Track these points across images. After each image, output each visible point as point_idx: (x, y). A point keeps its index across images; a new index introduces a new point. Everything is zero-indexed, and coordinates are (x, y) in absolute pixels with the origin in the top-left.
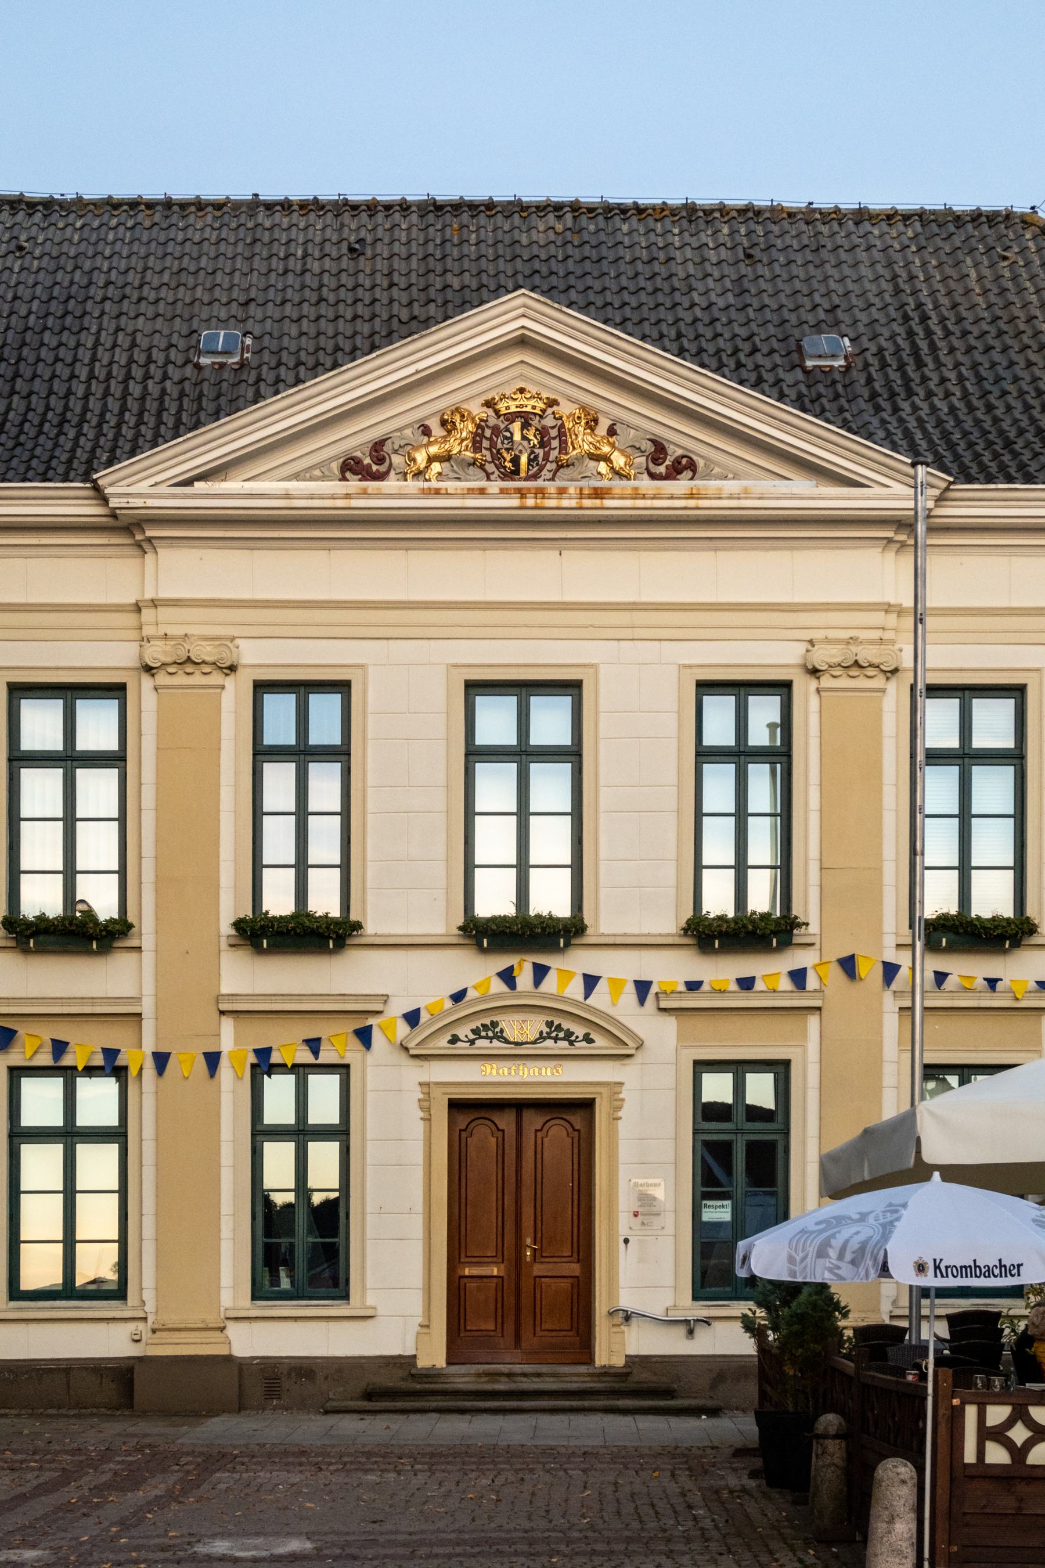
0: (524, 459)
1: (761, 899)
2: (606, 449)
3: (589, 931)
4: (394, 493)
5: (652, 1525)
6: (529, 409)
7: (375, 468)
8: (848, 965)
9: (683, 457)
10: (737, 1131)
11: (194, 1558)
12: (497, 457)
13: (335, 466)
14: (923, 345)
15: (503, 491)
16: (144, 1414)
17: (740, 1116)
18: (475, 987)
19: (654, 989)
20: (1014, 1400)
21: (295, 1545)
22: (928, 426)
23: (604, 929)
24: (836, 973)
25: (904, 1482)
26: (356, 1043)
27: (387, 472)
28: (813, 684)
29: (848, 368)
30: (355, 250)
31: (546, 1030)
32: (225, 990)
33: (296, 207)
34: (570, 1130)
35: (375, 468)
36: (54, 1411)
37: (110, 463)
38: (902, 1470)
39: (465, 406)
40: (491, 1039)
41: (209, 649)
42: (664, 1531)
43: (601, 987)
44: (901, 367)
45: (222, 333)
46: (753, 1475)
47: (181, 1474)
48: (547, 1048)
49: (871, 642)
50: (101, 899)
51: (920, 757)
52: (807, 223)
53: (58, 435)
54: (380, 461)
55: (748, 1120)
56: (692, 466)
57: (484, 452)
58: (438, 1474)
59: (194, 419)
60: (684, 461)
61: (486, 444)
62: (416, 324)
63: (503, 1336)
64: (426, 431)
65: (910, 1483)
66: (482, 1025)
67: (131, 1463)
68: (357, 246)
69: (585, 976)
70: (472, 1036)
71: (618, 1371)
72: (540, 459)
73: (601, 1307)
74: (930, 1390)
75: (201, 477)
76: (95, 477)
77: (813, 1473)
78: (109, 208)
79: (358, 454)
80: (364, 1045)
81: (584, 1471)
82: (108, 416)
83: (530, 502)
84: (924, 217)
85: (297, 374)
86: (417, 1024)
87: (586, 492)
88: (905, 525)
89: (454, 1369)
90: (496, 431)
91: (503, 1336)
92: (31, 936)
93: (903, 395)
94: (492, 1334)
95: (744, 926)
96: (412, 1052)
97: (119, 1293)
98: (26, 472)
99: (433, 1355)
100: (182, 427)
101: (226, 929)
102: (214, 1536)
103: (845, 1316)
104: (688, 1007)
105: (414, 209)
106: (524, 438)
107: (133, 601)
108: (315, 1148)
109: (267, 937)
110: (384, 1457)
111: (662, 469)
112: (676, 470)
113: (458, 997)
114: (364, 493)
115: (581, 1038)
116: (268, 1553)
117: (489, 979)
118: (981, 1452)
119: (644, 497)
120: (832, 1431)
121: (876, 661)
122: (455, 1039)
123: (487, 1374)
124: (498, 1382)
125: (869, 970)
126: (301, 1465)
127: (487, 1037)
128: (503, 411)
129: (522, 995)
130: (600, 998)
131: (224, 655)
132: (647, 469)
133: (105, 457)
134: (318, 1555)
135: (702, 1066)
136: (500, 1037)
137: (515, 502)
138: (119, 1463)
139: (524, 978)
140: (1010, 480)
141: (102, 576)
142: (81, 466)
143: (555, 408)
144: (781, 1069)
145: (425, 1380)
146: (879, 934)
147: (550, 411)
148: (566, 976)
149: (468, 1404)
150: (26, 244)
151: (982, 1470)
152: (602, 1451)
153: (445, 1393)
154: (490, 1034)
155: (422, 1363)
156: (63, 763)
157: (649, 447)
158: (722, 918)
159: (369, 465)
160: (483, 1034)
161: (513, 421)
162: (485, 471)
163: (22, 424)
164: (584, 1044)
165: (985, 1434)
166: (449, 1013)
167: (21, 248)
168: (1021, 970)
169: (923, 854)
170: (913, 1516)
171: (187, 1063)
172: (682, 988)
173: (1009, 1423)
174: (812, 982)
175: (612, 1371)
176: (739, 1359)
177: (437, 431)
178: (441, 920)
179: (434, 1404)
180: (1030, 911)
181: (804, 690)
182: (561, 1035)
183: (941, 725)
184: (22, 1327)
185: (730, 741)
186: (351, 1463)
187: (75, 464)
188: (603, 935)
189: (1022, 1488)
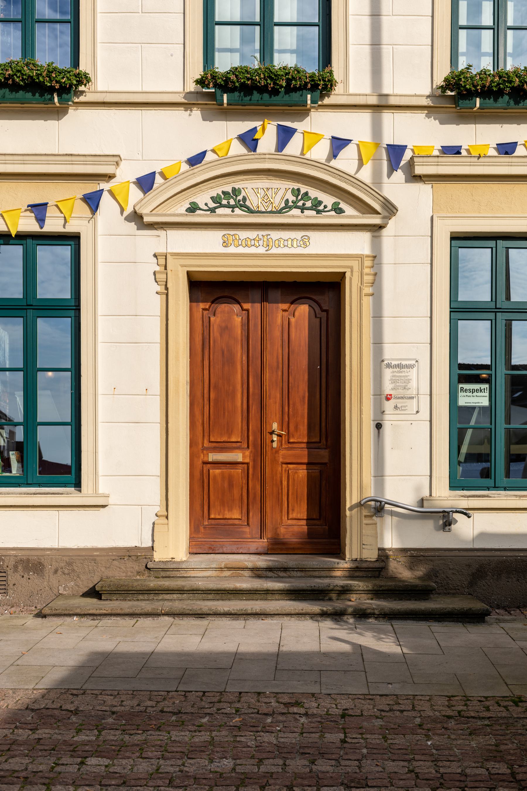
3: (338, 89)
18: (213, 151)
19: (407, 155)
26: (84, 209)
31: (291, 198)
40: (233, 207)
48: (293, 216)
63: (248, 524)
66: (223, 193)
70: (212, 205)
71: (371, 565)
73: (352, 497)
86: (151, 188)
91: (248, 524)
94: (237, 522)
96: (146, 219)
99: (174, 546)
108: (43, 326)
113: (196, 160)
115: (329, 207)
117: (229, 142)
122: (193, 208)
127: (228, 206)
129: (263, 157)
136: (243, 205)
139: (268, 140)
145: (163, 574)
153: (181, 591)
154: (232, 202)
155: (158, 556)
160: (224, 202)
166: (185, 175)
175: (365, 565)
176: (498, 553)
178: (174, 72)
182: (309, 204)
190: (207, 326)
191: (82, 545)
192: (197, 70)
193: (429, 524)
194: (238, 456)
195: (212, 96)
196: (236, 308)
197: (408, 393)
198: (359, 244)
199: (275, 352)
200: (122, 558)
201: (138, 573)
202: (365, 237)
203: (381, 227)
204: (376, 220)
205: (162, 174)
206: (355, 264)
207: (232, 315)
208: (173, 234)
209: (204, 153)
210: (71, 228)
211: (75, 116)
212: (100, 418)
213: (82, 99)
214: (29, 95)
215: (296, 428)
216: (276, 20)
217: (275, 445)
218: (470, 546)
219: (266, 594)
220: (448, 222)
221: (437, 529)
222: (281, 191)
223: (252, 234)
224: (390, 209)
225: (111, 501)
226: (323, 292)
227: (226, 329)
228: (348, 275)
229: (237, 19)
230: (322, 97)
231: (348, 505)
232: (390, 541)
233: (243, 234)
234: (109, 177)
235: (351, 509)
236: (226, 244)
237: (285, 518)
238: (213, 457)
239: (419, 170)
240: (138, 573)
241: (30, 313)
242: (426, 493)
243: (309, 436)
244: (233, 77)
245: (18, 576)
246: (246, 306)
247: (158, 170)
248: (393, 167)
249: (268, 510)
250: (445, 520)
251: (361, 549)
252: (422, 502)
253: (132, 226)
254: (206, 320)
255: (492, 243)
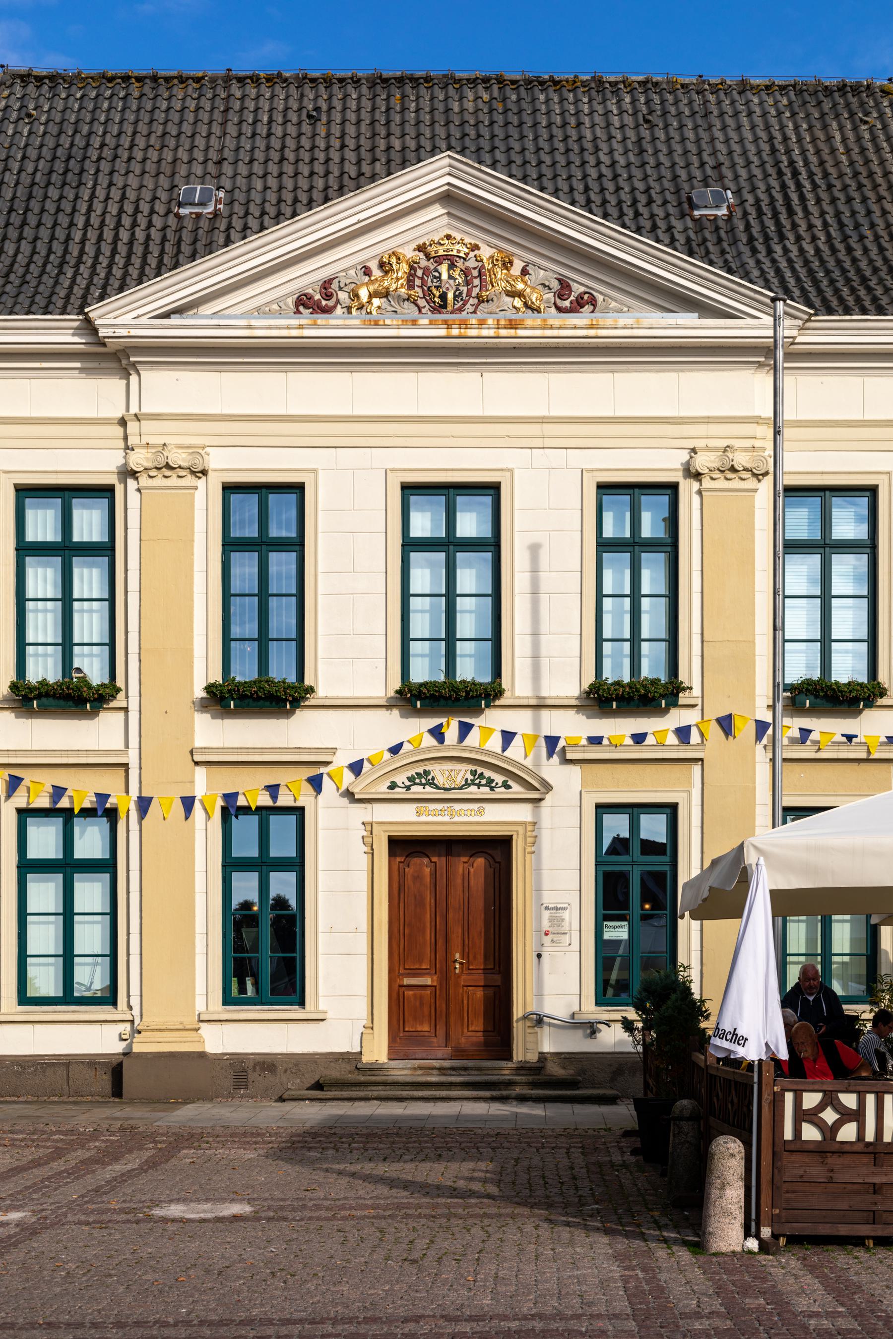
0: (450, 296)
1: (652, 666)
2: (520, 286)
4: (338, 327)
5: (538, 1193)
6: (455, 253)
7: (324, 303)
8: (726, 724)
9: (585, 293)
10: (633, 863)
11: (149, 1218)
12: (428, 293)
13: (290, 301)
14: (794, 197)
15: (432, 323)
16: (131, 1102)
17: (636, 848)
18: (409, 742)
19: (562, 743)
20: (825, 1088)
21: (236, 1209)
22: (797, 266)
23: (518, 692)
24: (714, 732)
25: (732, 1155)
26: (308, 789)
27: (335, 307)
28: (696, 486)
29: (730, 216)
30: (313, 117)
31: (470, 777)
32: (198, 743)
33: (264, 81)
34: (492, 862)
35: (324, 303)
36: (56, 1099)
37: (101, 298)
38: (731, 1145)
39: (400, 250)
40: (424, 785)
41: (184, 456)
42: (548, 1197)
43: (517, 741)
44: (776, 215)
45: (199, 187)
46: (634, 1152)
47: (154, 1151)
49: (745, 450)
50: (92, 667)
51: (780, 547)
52: (698, 93)
53: (58, 275)
54: (328, 297)
55: (643, 853)
56: (593, 302)
57: (417, 289)
58: (370, 1152)
59: (174, 260)
60: (586, 297)
61: (418, 282)
62: (361, 180)
64: (367, 272)
65: (738, 1157)
67: (112, 1142)
68: (314, 113)
69: (503, 732)
70: (408, 783)
72: (464, 295)
73: (518, 1011)
74: (756, 1079)
75: (179, 311)
76: (86, 310)
77: (670, 1150)
78: (104, 81)
79: (310, 291)
80: (315, 790)
81: (493, 1149)
82: (101, 258)
83: (455, 332)
84: (798, 88)
85: (262, 223)
87: (502, 322)
88: (769, 351)
89: (394, 1064)
90: (426, 271)
92: (34, 698)
93: (776, 240)
95: (638, 691)
96: (357, 796)
97: (110, 997)
98: (30, 306)
99: (377, 1051)
100: (164, 268)
101: (199, 693)
102: (171, 1201)
103: (707, 1018)
104: (593, 758)
105: (364, 81)
106: (450, 277)
107: (119, 415)
109: (233, 699)
110: (327, 1137)
111: (567, 304)
112: (579, 304)
113: (395, 750)
114: (315, 325)
116: (213, 1215)
117: (421, 735)
118: (797, 1131)
119: (551, 328)
120: (686, 1114)
121: (748, 466)
122: (393, 786)
123: (421, 1068)
124: (431, 1075)
125: (745, 730)
126: (256, 1143)
127: (420, 784)
128: (433, 254)
129: (448, 748)
130: (515, 751)
131: (197, 461)
132: (555, 304)
133: (97, 293)
134: (255, 1218)
135: (602, 809)
136: (432, 783)
137: (443, 332)
138: (103, 1141)
139: (452, 733)
140: (864, 311)
141: (103, 395)
142: (75, 301)
143: (476, 252)
144: (671, 810)
146: (752, 696)
147: (472, 254)
148: (487, 731)
149: (405, 1093)
150: (34, 112)
151: (799, 1146)
152: (511, 1132)
153: (385, 1084)
154: (423, 781)
155: (366, 1059)
156: (61, 552)
157: (555, 285)
158: (618, 683)
159: (319, 301)
160: (417, 781)
161: (441, 264)
162: (417, 305)
163: (28, 265)
164: (503, 789)
165: (801, 1116)
167: (29, 115)
168: (873, 725)
169: (783, 630)
170: (741, 1184)
171: (166, 806)
172: (584, 742)
173: (821, 1107)
174: (695, 738)
177: (377, 273)
178: (381, 683)
179: (375, 1094)
180: (883, 677)
181: (687, 490)
182: (484, 782)
183: (801, 522)
184: (29, 1027)
185: (274, 557)
186: (299, 1142)
187: (73, 299)
188: (518, 697)
189: (832, 1160)
190: (402, 875)
191: (305, 1051)
192: (397, 684)
193: (579, 1033)
194: (428, 981)
195: (409, 701)
196: (426, 861)
197: (562, 930)
198: (522, 813)
199: (457, 894)
200: (337, 1060)
201: (350, 1072)
202: (528, 807)
203: (541, 800)
204: (535, 795)
205: (369, 760)
206: (520, 829)
207: (423, 866)
208: (377, 806)
209: (401, 744)
210: (299, 804)
211: (301, 715)
212: (320, 951)
213: (307, 703)
214: (268, 703)
215: (475, 957)
216: (458, 636)
217: (457, 971)
218: (612, 1050)
219: (451, 1085)
220: (594, 795)
221: (586, 1036)
222: (463, 772)
223: (439, 806)
224: (548, 787)
225: (328, 1016)
226: (496, 850)
227: (418, 877)
228: (514, 838)
229: (427, 636)
230: (494, 700)
231: (515, 1018)
232: (547, 1047)
233: (432, 806)
234: (327, 763)
235: (517, 1021)
236: (418, 814)
237: (465, 1030)
238: (406, 981)
239: (569, 756)
240: (350, 1072)
241: (264, 868)
242: (576, 1008)
243: (485, 964)
244: (425, 691)
245: (256, 1074)
246: (434, 859)
247: (365, 757)
248: (550, 754)
249: (452, 1024)
250: (591, 1029)
251: (525, 1053)
252: (573, 1016)
253: (345, 801)
254: (402, 871)
255: (630, 810)
